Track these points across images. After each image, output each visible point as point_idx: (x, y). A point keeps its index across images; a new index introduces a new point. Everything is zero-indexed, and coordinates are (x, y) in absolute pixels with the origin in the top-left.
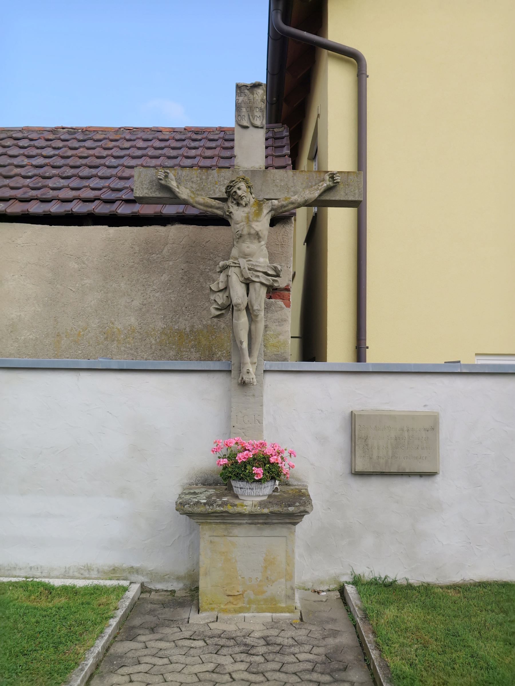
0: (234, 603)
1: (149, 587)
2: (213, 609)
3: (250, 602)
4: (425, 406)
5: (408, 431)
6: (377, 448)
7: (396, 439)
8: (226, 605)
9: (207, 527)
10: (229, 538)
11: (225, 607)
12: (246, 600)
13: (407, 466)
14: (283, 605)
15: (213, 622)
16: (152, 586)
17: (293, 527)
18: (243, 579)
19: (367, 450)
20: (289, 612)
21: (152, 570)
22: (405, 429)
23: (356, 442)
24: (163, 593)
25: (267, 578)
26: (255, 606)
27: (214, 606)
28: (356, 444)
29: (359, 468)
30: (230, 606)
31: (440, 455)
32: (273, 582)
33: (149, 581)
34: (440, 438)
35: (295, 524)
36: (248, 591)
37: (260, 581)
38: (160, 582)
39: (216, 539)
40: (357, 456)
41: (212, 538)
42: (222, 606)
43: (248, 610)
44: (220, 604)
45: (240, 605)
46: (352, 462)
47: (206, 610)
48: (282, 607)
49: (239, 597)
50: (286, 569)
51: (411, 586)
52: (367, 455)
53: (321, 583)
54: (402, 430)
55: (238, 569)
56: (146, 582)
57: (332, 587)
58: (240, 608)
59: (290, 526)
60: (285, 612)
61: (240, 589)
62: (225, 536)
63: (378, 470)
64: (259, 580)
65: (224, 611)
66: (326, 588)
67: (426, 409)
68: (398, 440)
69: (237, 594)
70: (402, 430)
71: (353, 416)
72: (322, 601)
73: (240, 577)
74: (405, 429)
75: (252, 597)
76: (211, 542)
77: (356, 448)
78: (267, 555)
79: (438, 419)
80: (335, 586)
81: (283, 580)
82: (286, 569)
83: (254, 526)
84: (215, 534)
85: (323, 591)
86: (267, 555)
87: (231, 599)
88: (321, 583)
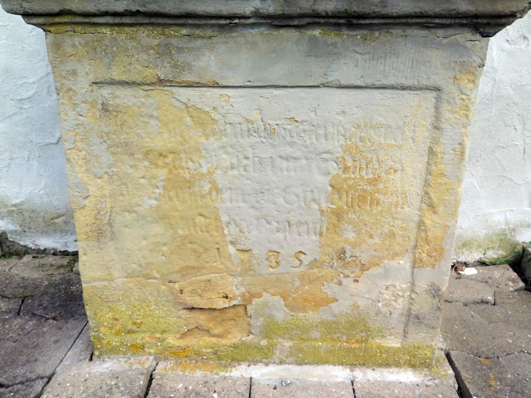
0: (216, 331)
1: (22, 243)
2: (138, 349)
3: (270, 330)
8: (184, 335)
9: (77, 40)
10: (183, 93)
11: (182, 343)
12: (258, 323)
14: (393, 343)
16: (27, 242)
17: (479, 41)
18: (243, 256)
20: (413, 366)
21: (22, 204)
24: (51, 260)
25: (341, 255)
26: (288, 344)
27: (138, 338)
30: (201, 342)
32: (364, 268)
33: (18, 228)
35: (489, 36)
36: (266, 296)
37: (314, 264)
38: (45, 233)
39: (125, 97)
41: (106, 91)
42: (172, 340)
43: (264, 356)
44: (163, 332)
45: (236, 337)
47: (113, 351)
48: (387, 350)
49: (230, 314)
50: (421, 224)
53: (464, 245)
55: (225, 219)
56: (12, 232)
57: (491, 255)
58: (235, 347)
59: (464, 37)
60: (398, 365)
61: (236, 287)
62: (161, 82)
64: (306, 260)
65: (180, 355)
66: (476, 256)
69: (222, 304)
72: (484, 302)
73: (231, 249)
75: (281, 314)
76: (105, 109)
78: (346, 169)
80: (501, 253)
81: (404, 263)
82: (421, 224)
83: (291, 34)
84: (116, 74)
85: (466, 265)
86: (346, 169)
87: (202, 318)
88: (464, 245)
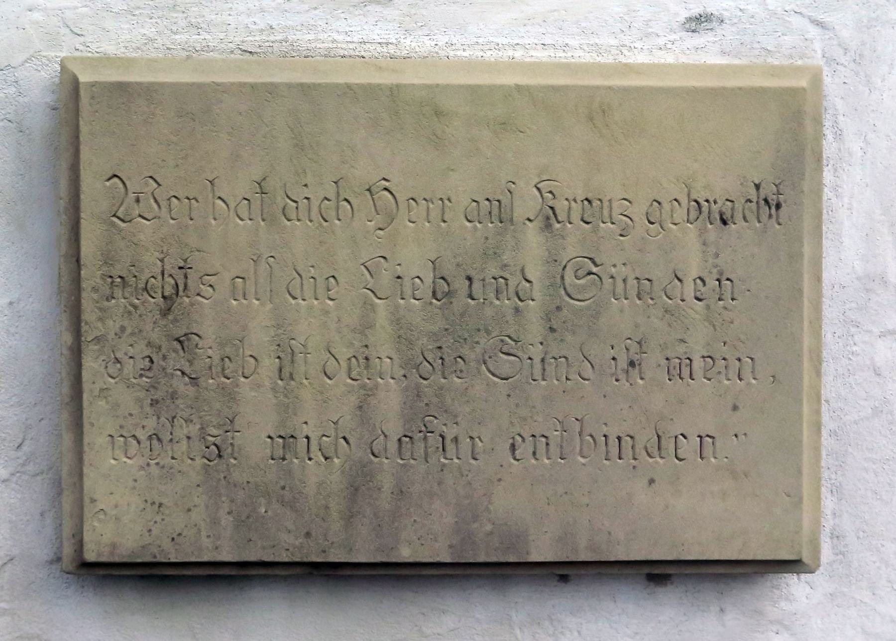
4: (699, 22)
5: (549, 219)
6: (269, 364)
7: (442, 293)
13: (532, 511)
15: (457, 449)
19: (181, 385)
22: (527, 204)
23: (89, 313)
28: (88, 334)
29: (117, 531)
31: (828, 423)
34: (827, 276)
40: (96, 438)
46: (67, 485)
51: (613, 89)
52: (182, 429)
54: (498, 212)
63: (287, 545)
67: (707, 52)
68: (461, 301)
70: (498, 212)
71: (72, 98)
74: (527, 204)
77: (91, 364)
79: (818, 122)
